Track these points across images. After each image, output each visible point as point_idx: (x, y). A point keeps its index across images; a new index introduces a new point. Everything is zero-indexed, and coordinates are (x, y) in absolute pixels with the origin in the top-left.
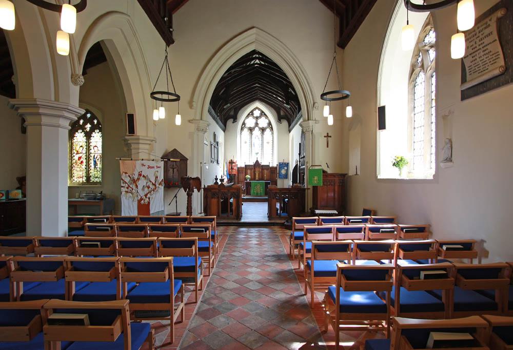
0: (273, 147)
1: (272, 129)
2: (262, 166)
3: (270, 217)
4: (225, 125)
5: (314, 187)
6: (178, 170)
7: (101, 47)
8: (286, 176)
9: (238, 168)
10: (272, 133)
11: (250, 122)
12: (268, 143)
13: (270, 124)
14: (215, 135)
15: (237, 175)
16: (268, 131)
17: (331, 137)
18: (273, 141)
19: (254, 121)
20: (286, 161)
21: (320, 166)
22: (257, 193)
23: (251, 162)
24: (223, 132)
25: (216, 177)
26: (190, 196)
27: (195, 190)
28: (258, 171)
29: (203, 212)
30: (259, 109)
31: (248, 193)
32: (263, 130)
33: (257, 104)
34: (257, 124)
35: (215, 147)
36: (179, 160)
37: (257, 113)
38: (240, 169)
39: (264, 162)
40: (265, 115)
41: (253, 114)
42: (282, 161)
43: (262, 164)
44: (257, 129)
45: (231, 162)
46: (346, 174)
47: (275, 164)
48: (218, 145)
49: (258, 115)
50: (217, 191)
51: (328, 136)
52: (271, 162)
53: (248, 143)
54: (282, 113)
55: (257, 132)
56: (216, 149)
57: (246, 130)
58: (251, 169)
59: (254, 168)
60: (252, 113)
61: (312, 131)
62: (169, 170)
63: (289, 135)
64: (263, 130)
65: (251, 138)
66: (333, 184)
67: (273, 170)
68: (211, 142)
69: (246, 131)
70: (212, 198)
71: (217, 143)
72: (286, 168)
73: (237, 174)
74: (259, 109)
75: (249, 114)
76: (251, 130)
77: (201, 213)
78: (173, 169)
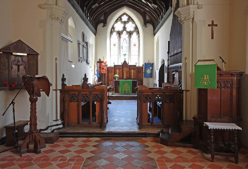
0: (139, 49)
1: (138, 33)
2: (130, 66)
3: (140, 125)
4: (96, 29)
5: (200, 90)
6: (25, 68)
7: (238, 156)
8: (151, 75)
9: (108, 68)
10: (139, 37)
11: (119, 27)
12: (135, 45)
13: (136, 28)
14: (83, 35)
15: (107, 74)
16: (135, 35)
17: (216, 25)
19: (122, 25)
20: (151, 62)
21: (213, 60)
22: (125, 91)
23: (120, 63)
24: (93, 36)
25: (63, 76)
26: (33, 101)
27: (43, 93)
29: (59, 118)
30: (127, 15)
31: (117, 91)
32: (130, 33)
33: (125, 10)
34: (125, 28)
35: (83, 46)
36: (26, 54)
37: (125, 18)
38: (109, 69)
39: (131, 63)
40: (132, 20)
41: (121, 19)
42: (147, 62)
43: (130, 64)
44: (125, 32)
45: (100, 62)
46: (244, 73)
47: (141, 65)
48: (87, 45)
49: (126, 20)
50: (77, 93)
51: (212, 25)
52: (137, 62)
53: (117, 46)
54: (147, 18)
55: (125, 35)
56: (85, 50)
57: (115, 34)
58: (119, 69)
60: (120, 18)
61: (193, 19)
62: (12, 68)
63: (153, 38)
64: (130, 33)
65: (120, 41)
66: (229, 85)
67: (139, 70)
68: (78, 41)
69: (115, 35)
70: (71, 101)
71: (87, 43)
72: (151, 68)
73: (106, 73)
74: (127, 15)
75: (117, 20)
76: (119, 33)
77: (57, 120)
78: (19, 66)
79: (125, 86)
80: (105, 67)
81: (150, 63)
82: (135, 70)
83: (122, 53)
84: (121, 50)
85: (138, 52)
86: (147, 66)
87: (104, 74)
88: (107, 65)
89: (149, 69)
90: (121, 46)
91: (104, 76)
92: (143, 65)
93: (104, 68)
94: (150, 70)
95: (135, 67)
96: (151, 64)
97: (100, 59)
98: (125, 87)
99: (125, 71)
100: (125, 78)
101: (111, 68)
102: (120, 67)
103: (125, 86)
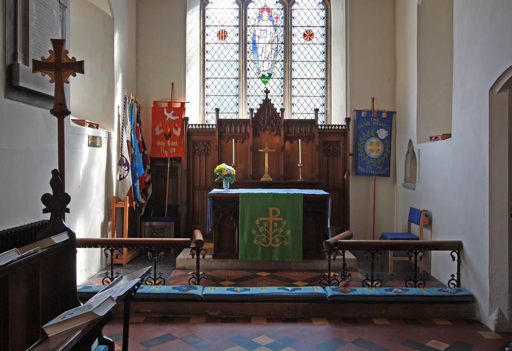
2: (290, 122)
15: (184, 160)
18: (328, 27)
28: (270, 143)
43: (287, 116)
47: (338, 118)
59: (256, 134)
72: (383, 133)
79: (266, 225)
80: (176, 129)
81: (380, 113)
82: (311, 143)
83: (255, 70)
84: (250, 56)
85: (323, 66)
86: (368, 124)
87: (171, 159)
88: (187, 119)
89: (376, 136)
90: (249, 39)
91: (174, 170)
92: (348, 120)
93: (171, 133)
94: (378, 144)
95: (311, 127)
96: (384, 115)
97: (59, 44)
98: (268, 228)
99: (266, 148)
100: (266, 178)
101: (203, 131)
102: (243, 128)
103: (266, 225)
